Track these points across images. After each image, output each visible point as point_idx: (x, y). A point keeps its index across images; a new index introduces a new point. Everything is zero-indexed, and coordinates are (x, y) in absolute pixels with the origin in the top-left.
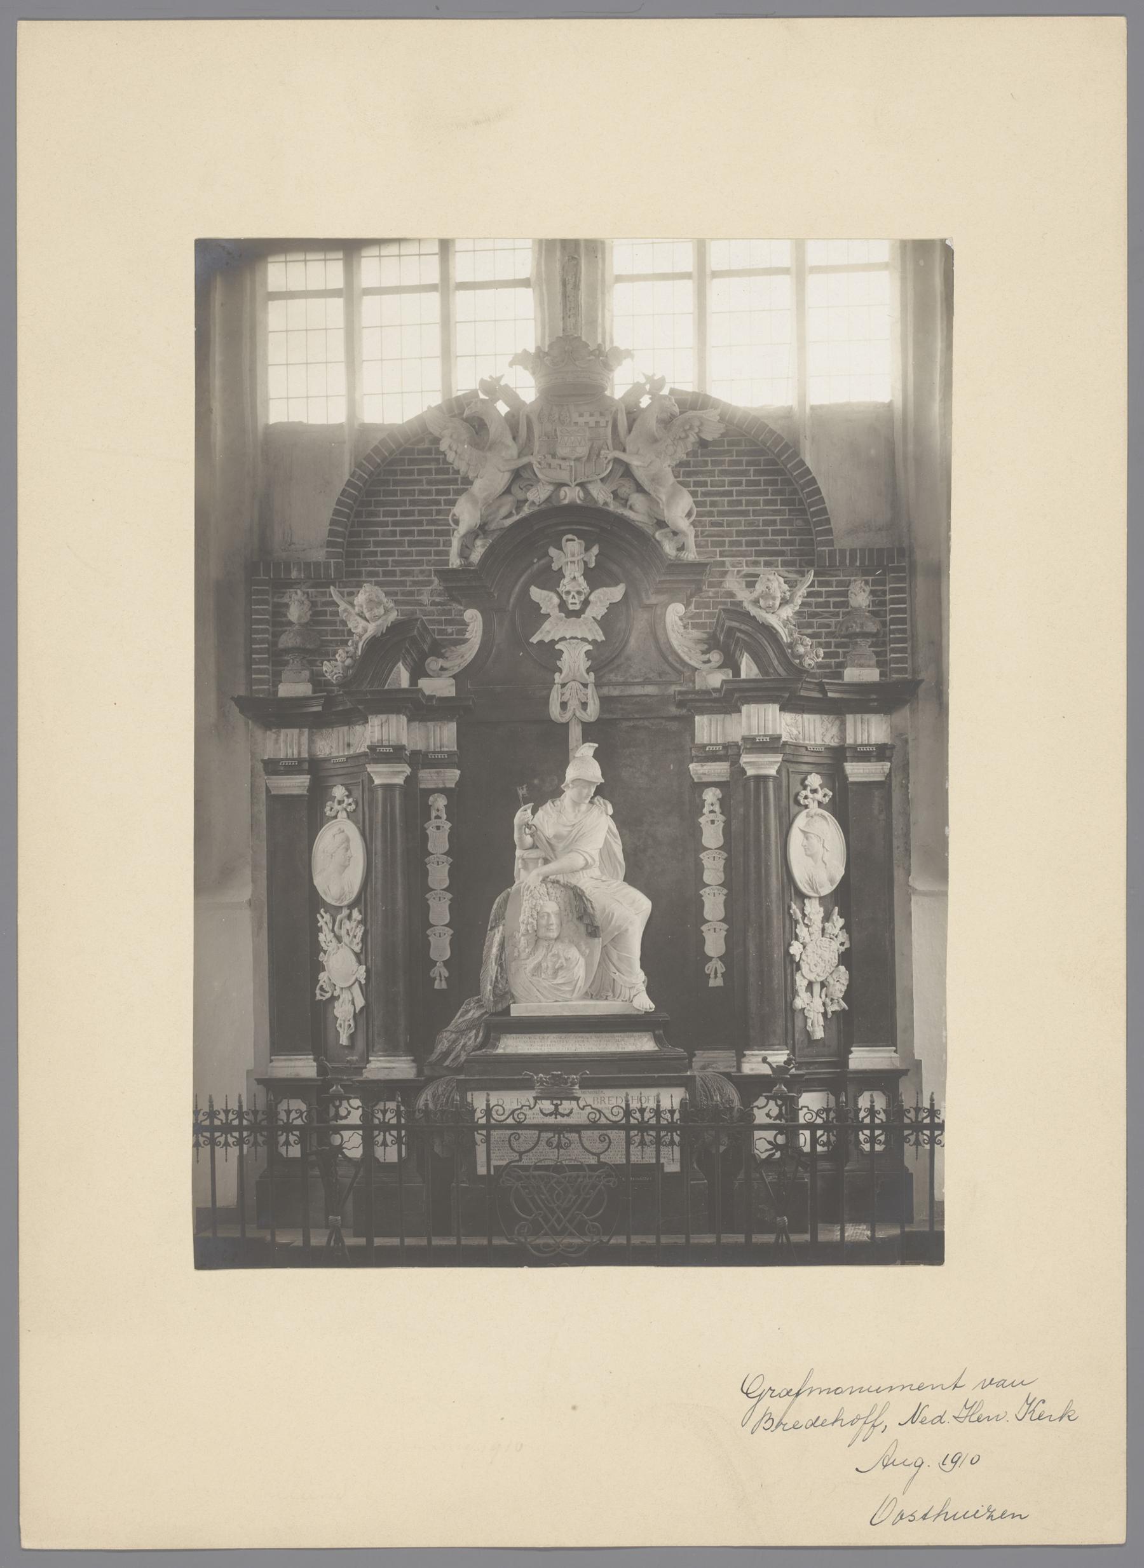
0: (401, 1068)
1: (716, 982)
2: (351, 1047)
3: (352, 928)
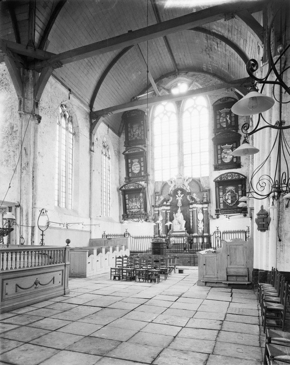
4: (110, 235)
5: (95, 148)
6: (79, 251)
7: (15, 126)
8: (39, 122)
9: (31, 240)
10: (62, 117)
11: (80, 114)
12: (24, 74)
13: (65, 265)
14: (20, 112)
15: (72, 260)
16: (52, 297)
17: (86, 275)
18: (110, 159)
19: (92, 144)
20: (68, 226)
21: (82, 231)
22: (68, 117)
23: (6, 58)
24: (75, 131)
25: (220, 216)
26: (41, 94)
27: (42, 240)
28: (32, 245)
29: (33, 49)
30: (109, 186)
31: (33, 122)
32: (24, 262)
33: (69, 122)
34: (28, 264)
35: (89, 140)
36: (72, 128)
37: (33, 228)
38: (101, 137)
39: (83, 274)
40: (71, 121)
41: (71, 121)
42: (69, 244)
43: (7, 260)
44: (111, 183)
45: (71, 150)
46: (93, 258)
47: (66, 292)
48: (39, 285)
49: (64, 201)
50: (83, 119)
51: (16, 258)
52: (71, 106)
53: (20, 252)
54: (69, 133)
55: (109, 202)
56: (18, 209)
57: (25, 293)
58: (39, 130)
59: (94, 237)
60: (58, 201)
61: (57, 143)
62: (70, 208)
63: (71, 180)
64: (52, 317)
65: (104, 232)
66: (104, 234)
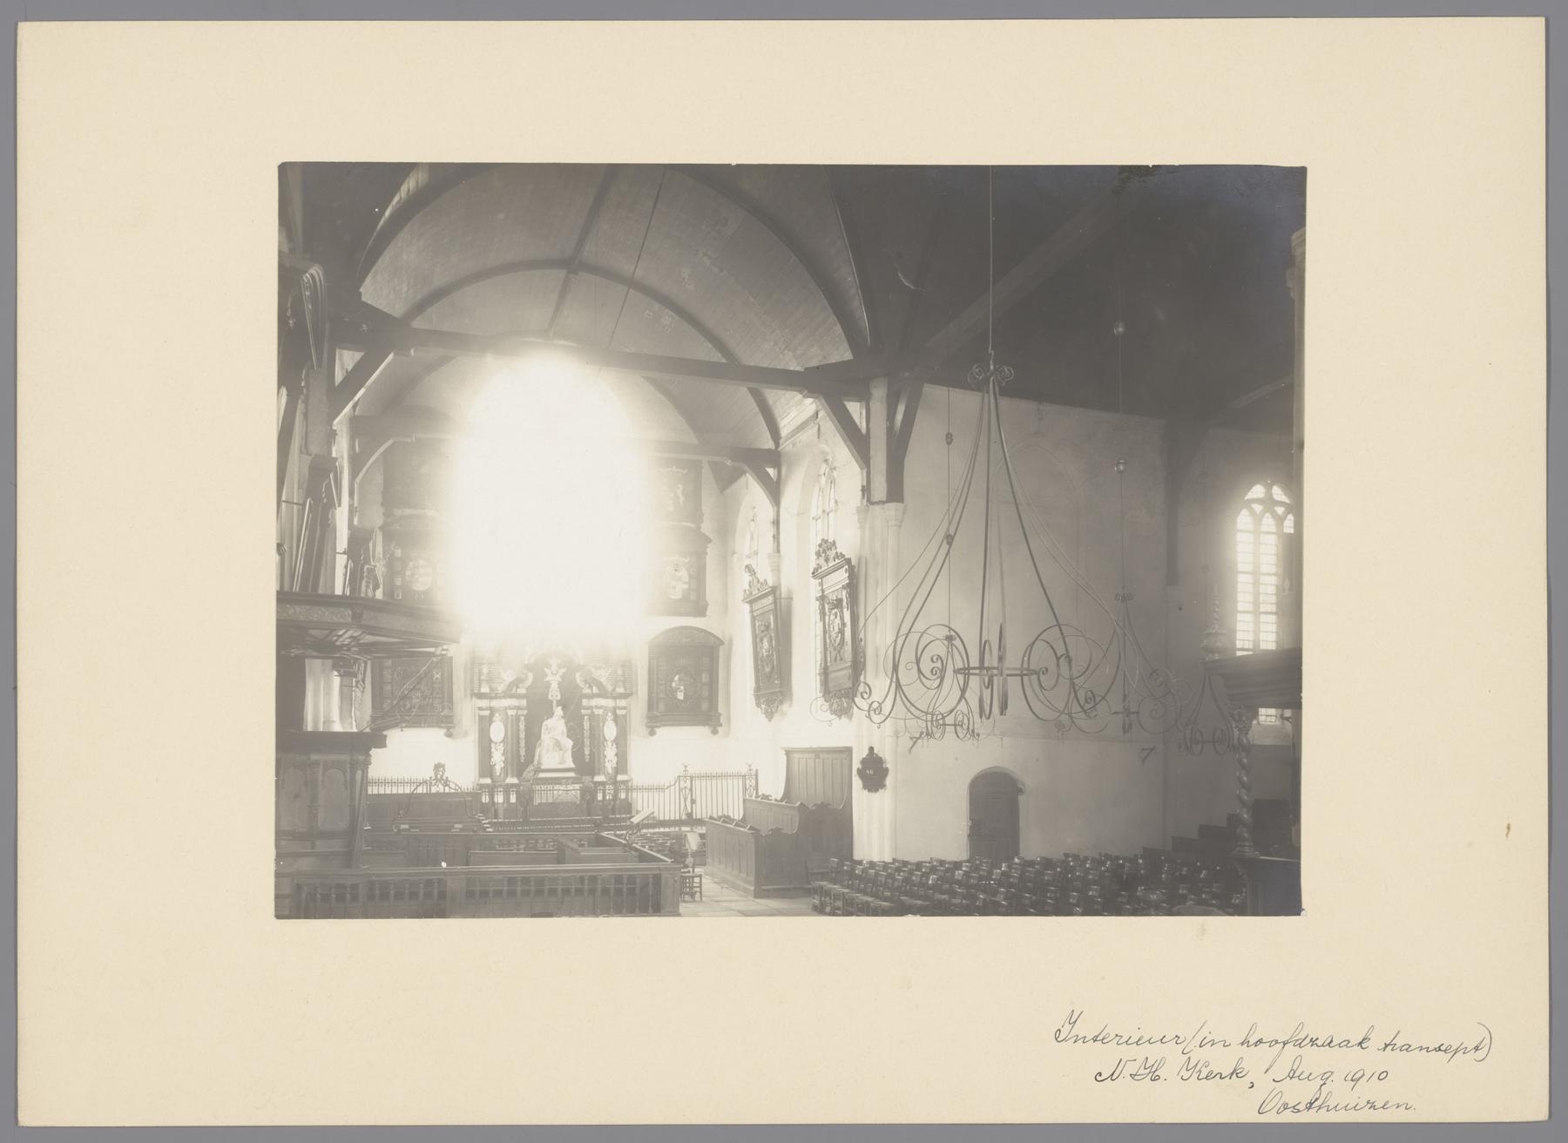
0: (515, 781)
1: (587, 760)
2: (500, 776)
3: (501, 747)
25: (657, 730)
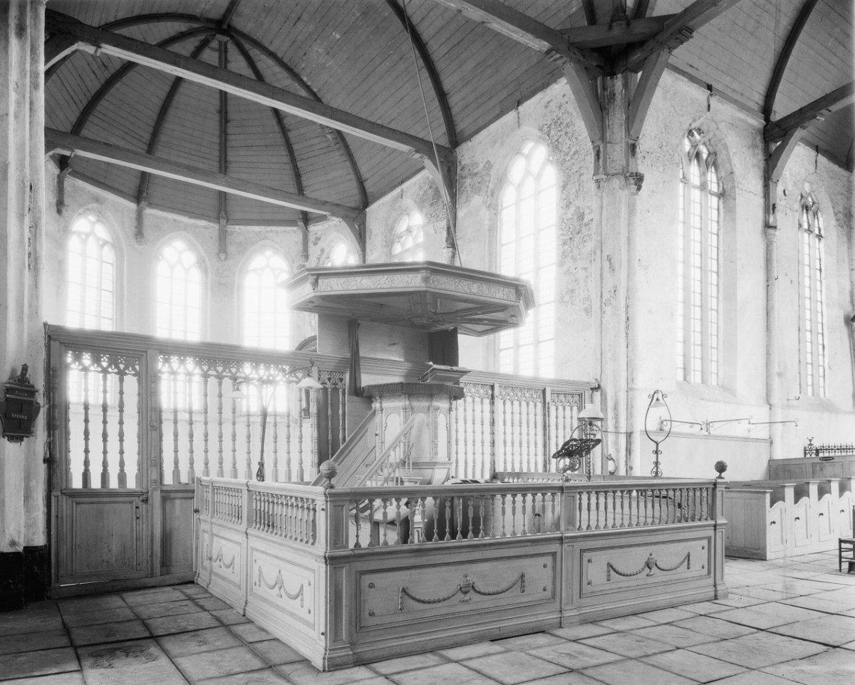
4: (829, 449)
5: (780, 218)
6: (745, 492)
7: (587, 211)
8: (639, 188)
9: (626, 464)
10: (690, 160)
11: (738, 138)
12: (604, 88)
13: (715, 526)
14: (598, 177)
15: (729, 511)
16: (686, 600)
17: (765, 556)
18: (823, 240)
19: (771, 207)
20: (711, 429)
21: (746, 439)
22: (705, 156)
23: (570, 68)
24: (725, 186)
26: (642, 121)
27: (657, 463)
28: (627, 477)
29: (624, 22)
30: (819, 315)
31: (626, 192)
32: (622, 514)
33: (708, 168)
34: (630, 519)
35: (762, 201)
36: (716, 181)
37: (629, 435)
38: (795, 184)
39: (756, 552)
40: (715, 164)
41: (715, 164)
42: (723, 475)
43: (589, 510)
44: (828, 305)
45: (716, 237)
46: (783, 511)
47: (719, 593)
48: (655, 569)
49: (698, 367)
50: (744, 149)
51: (606, 503)
52: (713, 126)
53: (614, 492)
54: (709, 196)
55: (821, 357)
56: (597, 395)
57: (626, 584)
58: (639, 207)
59: (780, 455)
60: (685, 369)
61: (681, 227)
62: (714, 383)
63: (714, 313)
64: (693, 649)
65: (810, 440)
66: (810, 445)
